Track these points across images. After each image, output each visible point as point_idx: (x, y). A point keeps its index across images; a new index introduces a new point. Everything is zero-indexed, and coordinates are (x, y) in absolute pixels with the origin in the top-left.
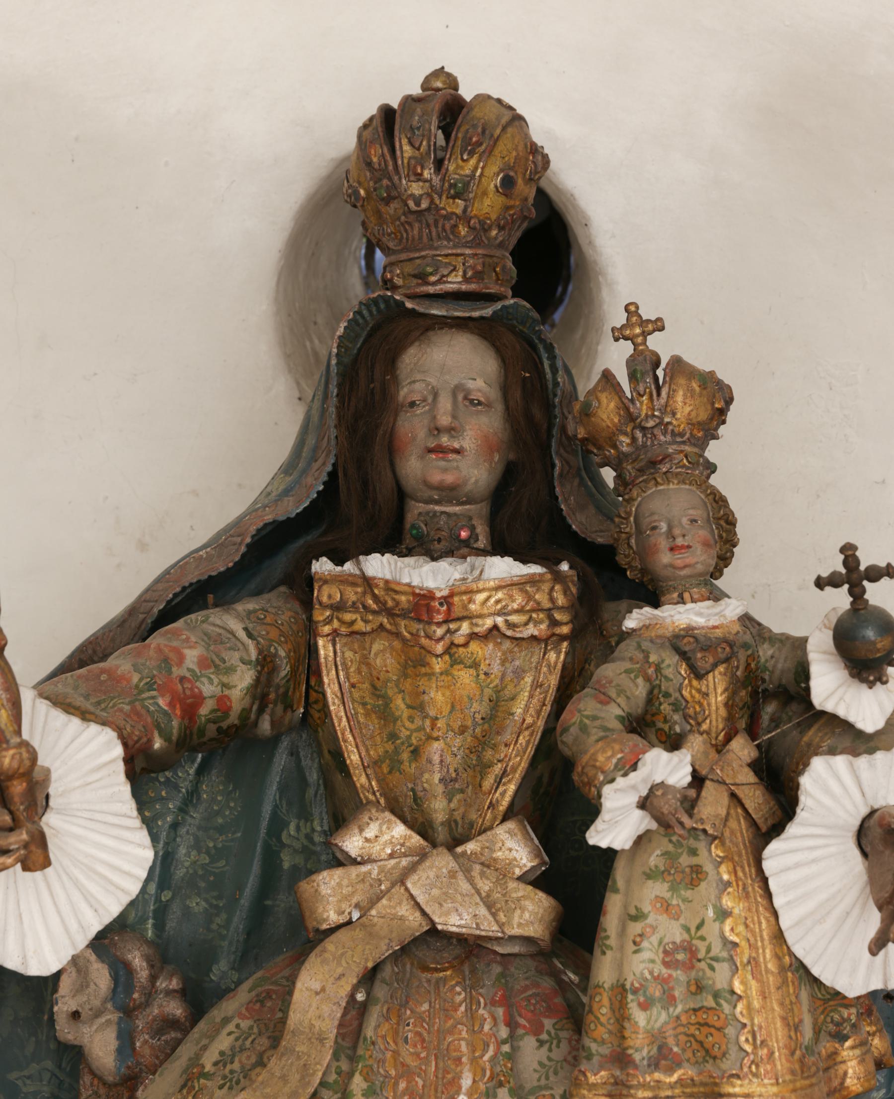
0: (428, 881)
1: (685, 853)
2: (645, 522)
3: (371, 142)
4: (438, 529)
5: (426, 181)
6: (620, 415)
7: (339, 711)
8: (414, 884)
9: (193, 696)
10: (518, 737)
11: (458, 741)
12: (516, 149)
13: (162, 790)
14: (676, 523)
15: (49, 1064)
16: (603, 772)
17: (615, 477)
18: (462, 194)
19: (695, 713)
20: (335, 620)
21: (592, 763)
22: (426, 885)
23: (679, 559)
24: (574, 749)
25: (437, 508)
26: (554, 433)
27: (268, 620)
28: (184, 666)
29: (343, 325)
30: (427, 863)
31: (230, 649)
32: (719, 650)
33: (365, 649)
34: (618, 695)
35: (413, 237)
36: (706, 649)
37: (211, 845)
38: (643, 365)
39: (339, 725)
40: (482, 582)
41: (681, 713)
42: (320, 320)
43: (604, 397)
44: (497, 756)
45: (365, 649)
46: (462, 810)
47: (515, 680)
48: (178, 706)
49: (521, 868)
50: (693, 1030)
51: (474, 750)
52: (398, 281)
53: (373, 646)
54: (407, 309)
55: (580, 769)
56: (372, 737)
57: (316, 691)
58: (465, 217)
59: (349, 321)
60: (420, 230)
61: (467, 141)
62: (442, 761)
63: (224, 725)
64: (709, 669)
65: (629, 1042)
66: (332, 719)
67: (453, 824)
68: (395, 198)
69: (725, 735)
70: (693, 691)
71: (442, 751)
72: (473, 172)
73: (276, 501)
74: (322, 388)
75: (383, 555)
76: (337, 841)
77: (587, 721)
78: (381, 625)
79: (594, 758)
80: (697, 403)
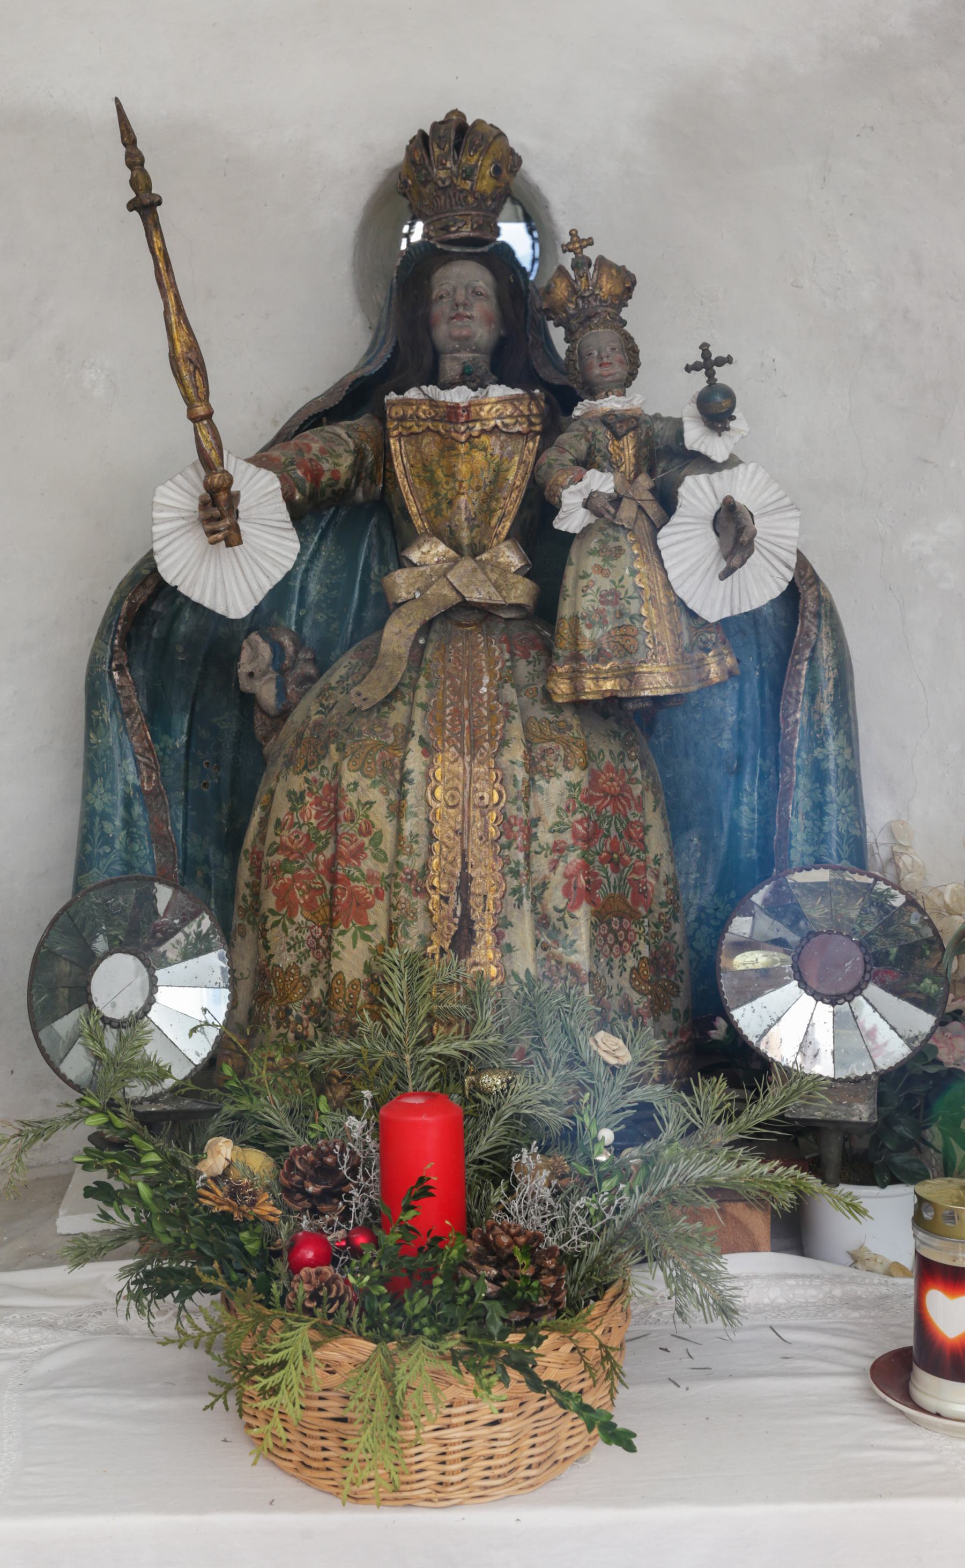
11: (476, 495)
15: (236, 712)
38: (581, 264)
50: (618, 639)
61: (473, 143)
63: (336, 488)
65: (581, 647)
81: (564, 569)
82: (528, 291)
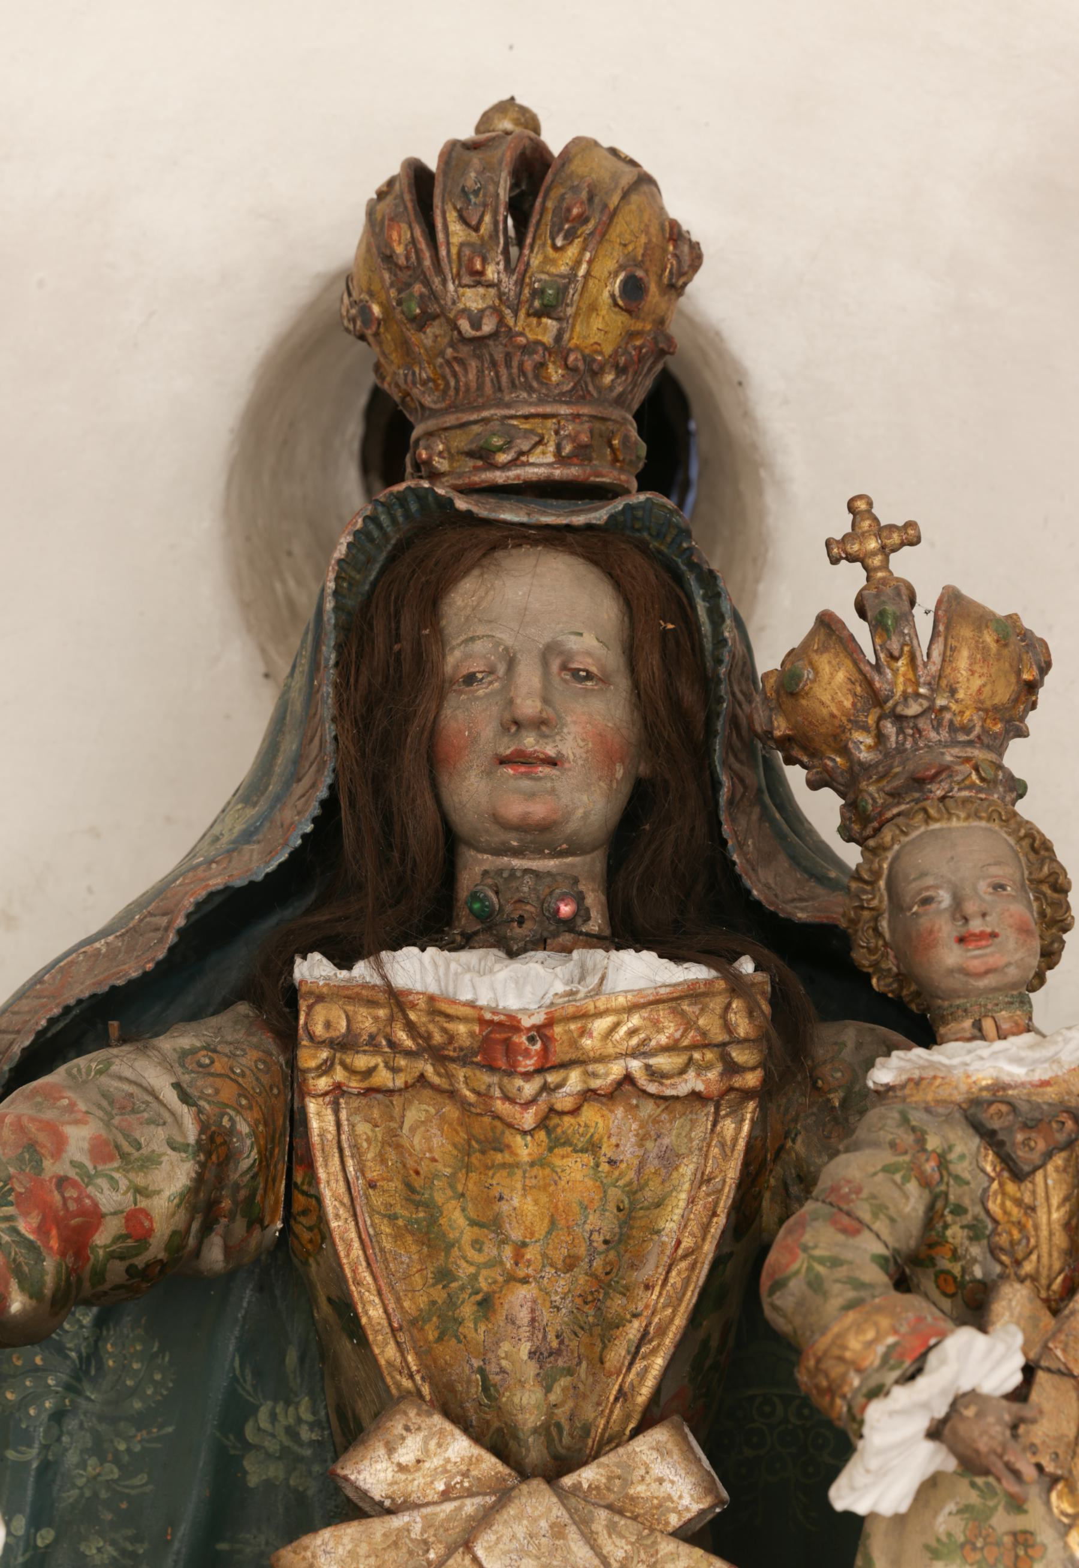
0: (515, 1545)
1: (1000, 1508)
2: (910, 890)
3: (391, 219)
4: (520, 901)
5: (490, 285)
6: (855, 695)
7: (347, 1230)
8: (489, 1549)
9: (82, 1212)
10: (668, 1272)
11: (562, 1284)
12: (646, 232)
13: (36, 1354)
14: (968, 891)
16: (859, 1371)
17: (843, 807)
18: (554, 307)
19: (1012, 1243)
20: (338, 1068)
21: (836, 1352)
22: (510, 1552)
23: (975, 958)
24: (798, 1321)
25: (516, 863)
26: (719, 728)
27: (218, 1067)
28: (66, 1157)
29: (345, 540)
30: (512, 1510)
31: (151, 1122)
32: (1054, 1125)
33: (392, 1118)
34: (875, 1216)
35: (467, 384)
36: (1030, 1125)
37: (122, 1447)
39: (348, 1255)
40: (603, 998)
41: (985, 1242)
42: (297, 549)
43: (824, 663)
44: (632, 1308)
45: (392, 1118)
46: (570, 1404)
47: (663, 1171)
48: (54, 1232)
49: (679, 1513)
51: (590, 1298)
52: (441, 464)
53: (408, 1114)
54: (457, 511)
55: (812, 1363)
56: (407, 1277)
57: (305, 1194)
58: (559, 350)
59: (356, 534)
60: (480, 372)
61: (563, 214)
62: (533, 1320)
63: (140, 1261)
64: (1038, 1162)
66: (334, 1244)
67: (554, 1431)
68: (435, 317)
69: (1064, 1280)
70: (1009, 1204)
71: (534, 1301)
72: (572, 269)
73: (230, 852)
74: (307, 653)
75: (423, 950)
76: (346, 1472)
77: (820, 1269)
78: (422, 1076)
79: (840, 1341)
80: (993, 670)
82: (720, 642)
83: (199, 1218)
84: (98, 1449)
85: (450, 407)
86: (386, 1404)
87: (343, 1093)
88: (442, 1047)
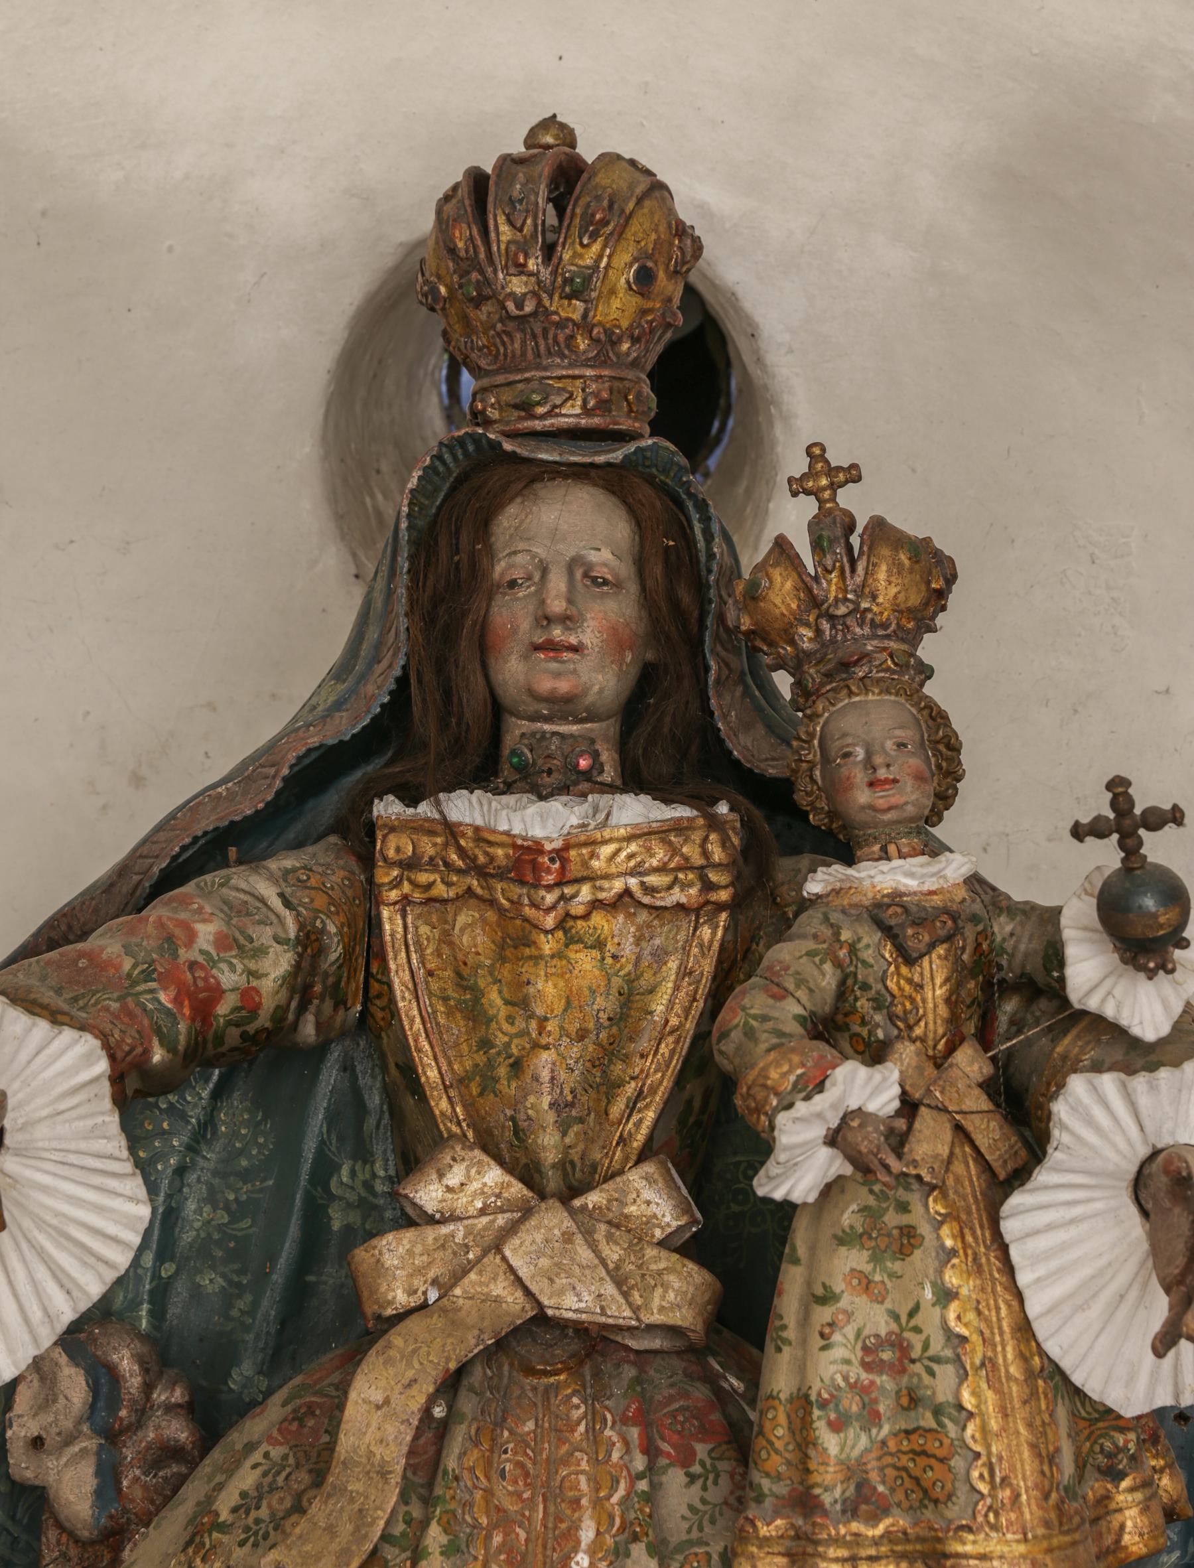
0: (534, 1247)
2: (834, 747)
4: (548, 756)
5: (531, 274)
8: (514, 1250)
9: (208, 988)
11: (575, 1051)
16: (777, 1094)
18: (581, 292)
19: (905, 1012)
21: (761, 1081)
25: (547, 727)
27: (313, 882)
29: (417, 474)
30: (533, 1222)
31: (260, 922)
33: (446, 922)
34: (798, 987)
35: (513, 351)
36: (918, 923)
37: (231, 1197)
43: (777, 574)
44: (630, 1071)
45: (446, 922)
46: (581, 1146)
47: (655, 966)
48: (186, 1003)
49: (662, 1228)
50: (904, 1460)
52: (493, 414)
56: (457, 1045)
57: (379, 981)
58: (585, 325)
59: (425, 469)
60: (523, 342)
61: (588, 219)
62: (553, 1078)
63: (251, 1028)
66: (401, 1020)
68: (488, 298)
73: (324, 718)
74: (387, 561)
77: (754, 1023)
81: (777, 1270)
83: (297, 998)
84: (212, 1198)
85: (500, 369)
86: (439, 1141)
87: (410, 903)
88: (485, 866)
